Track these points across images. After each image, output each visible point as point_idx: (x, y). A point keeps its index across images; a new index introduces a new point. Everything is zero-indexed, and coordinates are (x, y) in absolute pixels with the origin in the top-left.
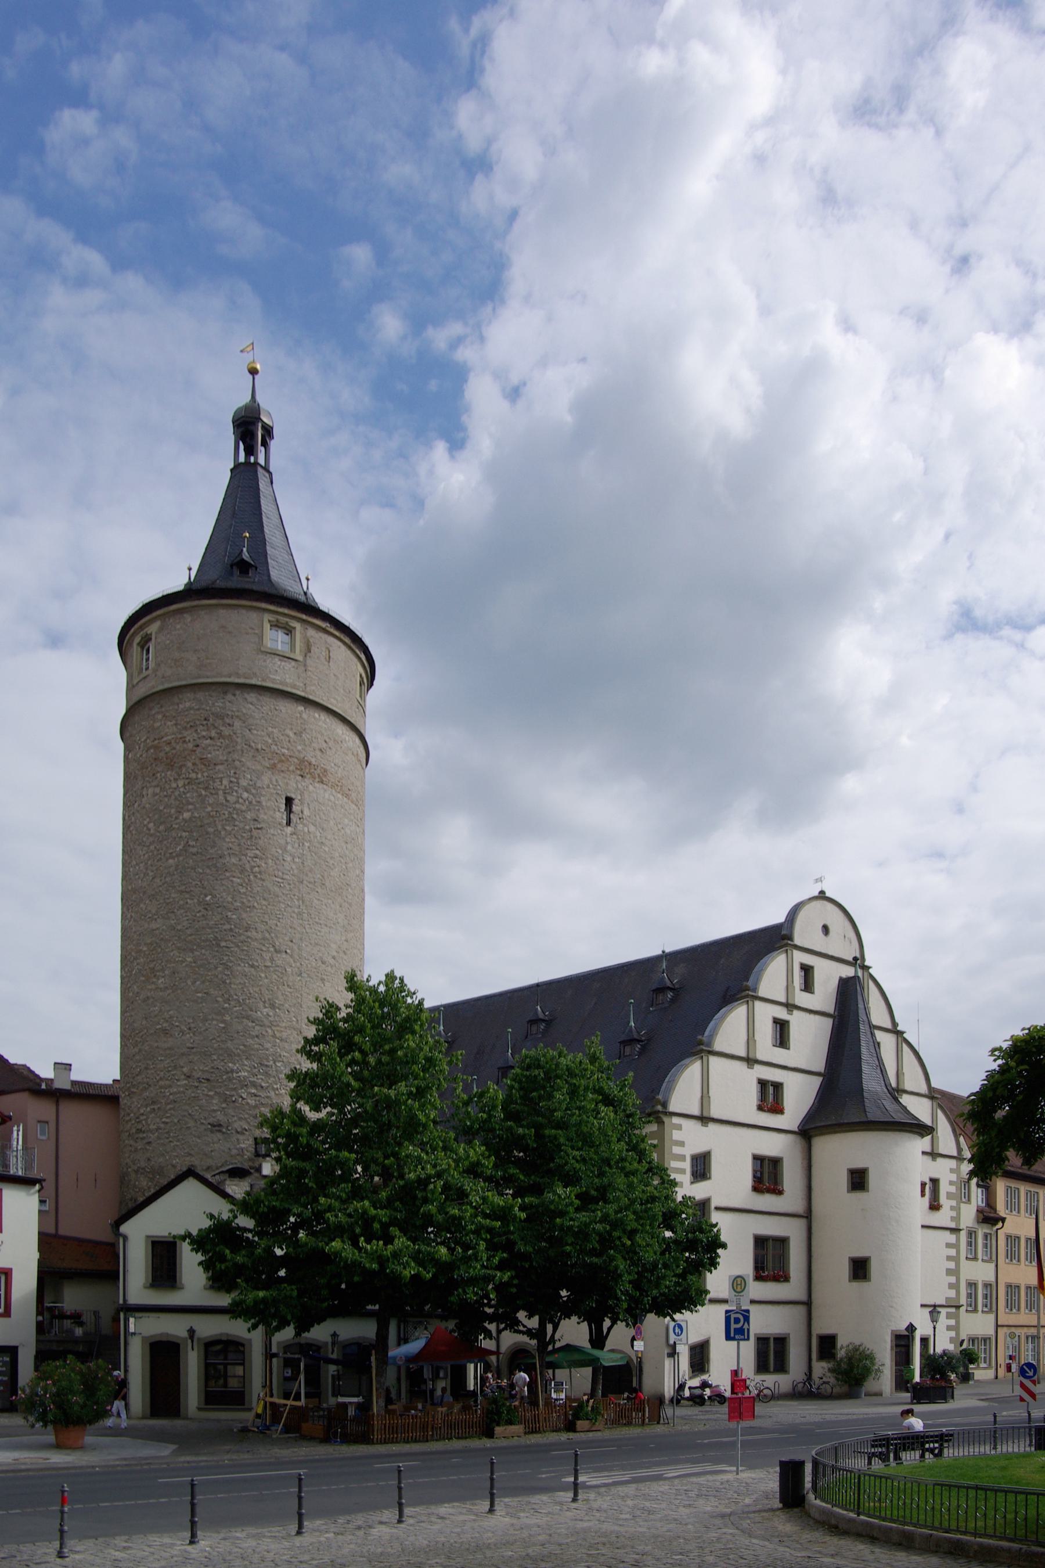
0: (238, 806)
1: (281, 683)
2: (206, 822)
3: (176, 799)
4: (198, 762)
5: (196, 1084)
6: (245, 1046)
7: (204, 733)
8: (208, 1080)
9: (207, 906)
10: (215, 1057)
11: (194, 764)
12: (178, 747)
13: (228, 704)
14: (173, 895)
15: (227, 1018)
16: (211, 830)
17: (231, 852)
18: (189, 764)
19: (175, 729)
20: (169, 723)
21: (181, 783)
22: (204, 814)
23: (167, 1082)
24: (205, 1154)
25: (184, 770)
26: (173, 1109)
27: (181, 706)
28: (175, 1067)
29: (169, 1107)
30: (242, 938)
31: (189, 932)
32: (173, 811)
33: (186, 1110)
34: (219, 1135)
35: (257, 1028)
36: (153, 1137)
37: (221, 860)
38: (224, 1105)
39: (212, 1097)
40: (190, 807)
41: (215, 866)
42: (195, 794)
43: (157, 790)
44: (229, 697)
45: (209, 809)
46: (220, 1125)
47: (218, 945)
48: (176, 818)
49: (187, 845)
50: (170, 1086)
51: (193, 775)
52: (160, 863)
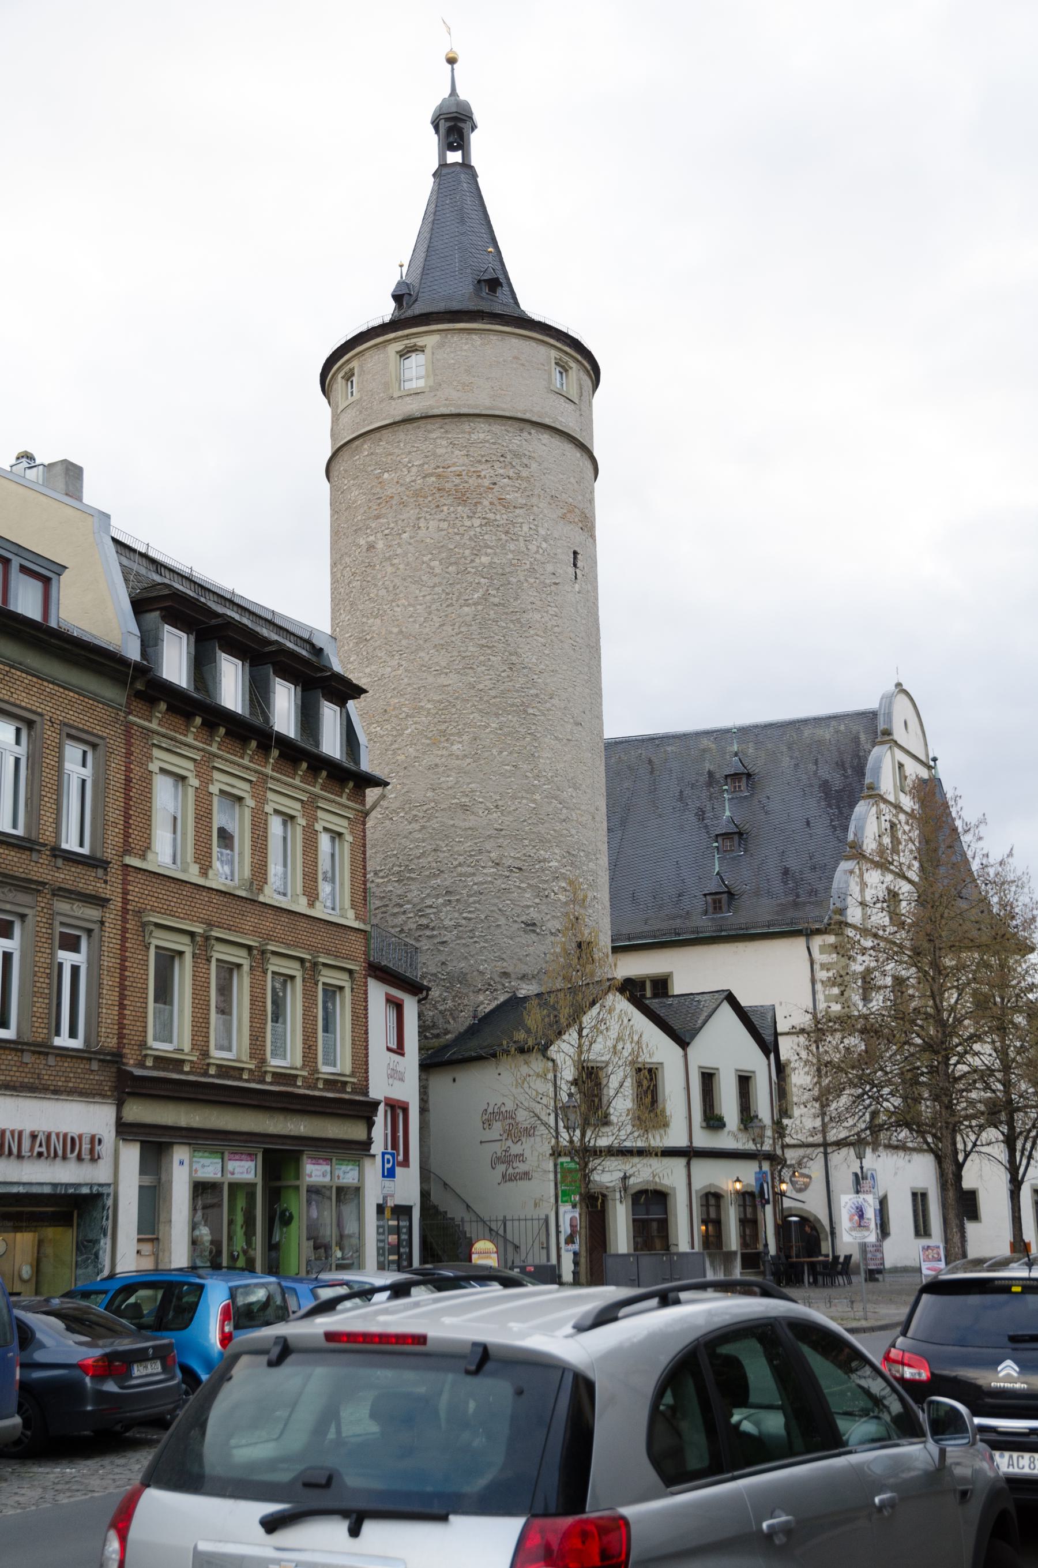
0: (538, 556)
1: (490, 408)
2: (508, 570)
3: (471, 539)
4: (496, 502)
5: (507, 874)
6: (554, 830)
7: (501, 471)
8: (520, 869)
9: (512, 666)
10: (526, 842)
11: (491, 503)
12: (470, 481)
13: (524, 443)
14: (471, 649)
15: (537, 797)
16: (513, 580)
17: (534, 606)
18: (486, 503)
19: (467, 461)
20: (457, 452)
21: (477, 522)
22: (504, 561)
23: (470, 870)
24: (520, 960)
25: (479, 508)
26: (479, 902)
27: (474, 437)
28: (480, 852)
29: (471, 900)
30: (548, 705)
31: (493, 693)
32: (467, 552)
33: (495, 905)
34: (533, 936)
35: (565, 811)
36: (448, 937)
37: (525, 615)
38: (537, 901)
39: (524, 890)
40: (489, 551)
41: (518, 620)
42: (494, 538)
43: (444, 525)
44: (525, 435)
45: (510, 556)
46: (534, 924)
47: (525, 711)
48: (472, 561)
49: (487, 594)
50: (474, 874)
51: (491, 516)
52: (450, 609)
